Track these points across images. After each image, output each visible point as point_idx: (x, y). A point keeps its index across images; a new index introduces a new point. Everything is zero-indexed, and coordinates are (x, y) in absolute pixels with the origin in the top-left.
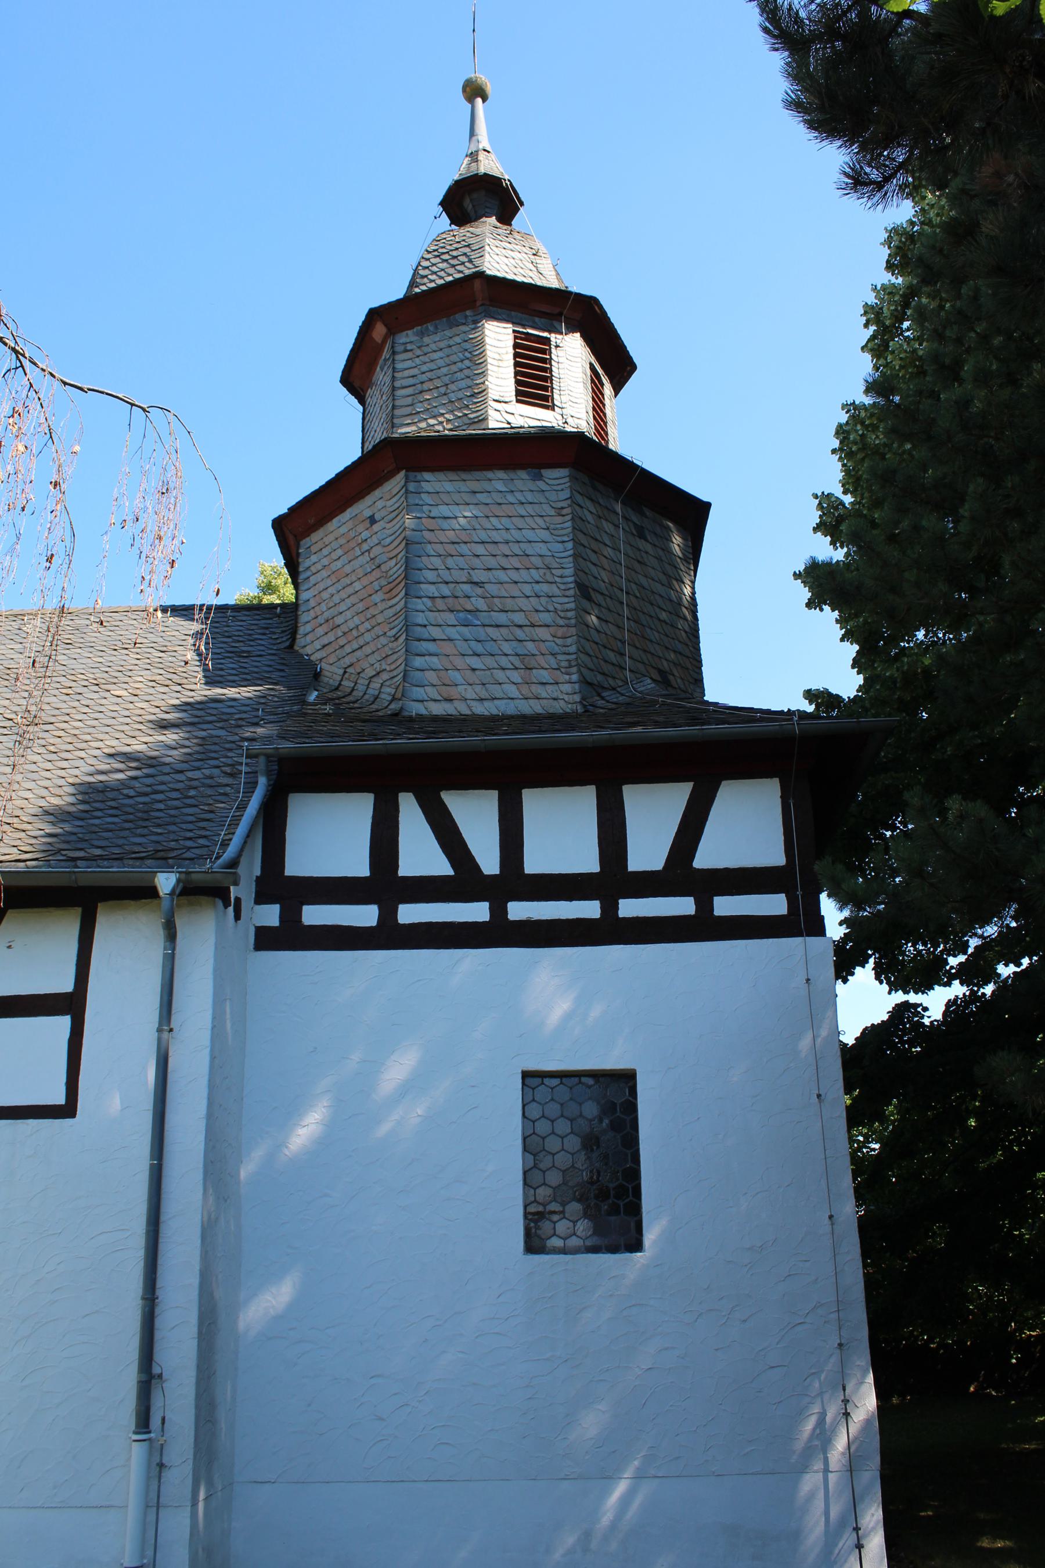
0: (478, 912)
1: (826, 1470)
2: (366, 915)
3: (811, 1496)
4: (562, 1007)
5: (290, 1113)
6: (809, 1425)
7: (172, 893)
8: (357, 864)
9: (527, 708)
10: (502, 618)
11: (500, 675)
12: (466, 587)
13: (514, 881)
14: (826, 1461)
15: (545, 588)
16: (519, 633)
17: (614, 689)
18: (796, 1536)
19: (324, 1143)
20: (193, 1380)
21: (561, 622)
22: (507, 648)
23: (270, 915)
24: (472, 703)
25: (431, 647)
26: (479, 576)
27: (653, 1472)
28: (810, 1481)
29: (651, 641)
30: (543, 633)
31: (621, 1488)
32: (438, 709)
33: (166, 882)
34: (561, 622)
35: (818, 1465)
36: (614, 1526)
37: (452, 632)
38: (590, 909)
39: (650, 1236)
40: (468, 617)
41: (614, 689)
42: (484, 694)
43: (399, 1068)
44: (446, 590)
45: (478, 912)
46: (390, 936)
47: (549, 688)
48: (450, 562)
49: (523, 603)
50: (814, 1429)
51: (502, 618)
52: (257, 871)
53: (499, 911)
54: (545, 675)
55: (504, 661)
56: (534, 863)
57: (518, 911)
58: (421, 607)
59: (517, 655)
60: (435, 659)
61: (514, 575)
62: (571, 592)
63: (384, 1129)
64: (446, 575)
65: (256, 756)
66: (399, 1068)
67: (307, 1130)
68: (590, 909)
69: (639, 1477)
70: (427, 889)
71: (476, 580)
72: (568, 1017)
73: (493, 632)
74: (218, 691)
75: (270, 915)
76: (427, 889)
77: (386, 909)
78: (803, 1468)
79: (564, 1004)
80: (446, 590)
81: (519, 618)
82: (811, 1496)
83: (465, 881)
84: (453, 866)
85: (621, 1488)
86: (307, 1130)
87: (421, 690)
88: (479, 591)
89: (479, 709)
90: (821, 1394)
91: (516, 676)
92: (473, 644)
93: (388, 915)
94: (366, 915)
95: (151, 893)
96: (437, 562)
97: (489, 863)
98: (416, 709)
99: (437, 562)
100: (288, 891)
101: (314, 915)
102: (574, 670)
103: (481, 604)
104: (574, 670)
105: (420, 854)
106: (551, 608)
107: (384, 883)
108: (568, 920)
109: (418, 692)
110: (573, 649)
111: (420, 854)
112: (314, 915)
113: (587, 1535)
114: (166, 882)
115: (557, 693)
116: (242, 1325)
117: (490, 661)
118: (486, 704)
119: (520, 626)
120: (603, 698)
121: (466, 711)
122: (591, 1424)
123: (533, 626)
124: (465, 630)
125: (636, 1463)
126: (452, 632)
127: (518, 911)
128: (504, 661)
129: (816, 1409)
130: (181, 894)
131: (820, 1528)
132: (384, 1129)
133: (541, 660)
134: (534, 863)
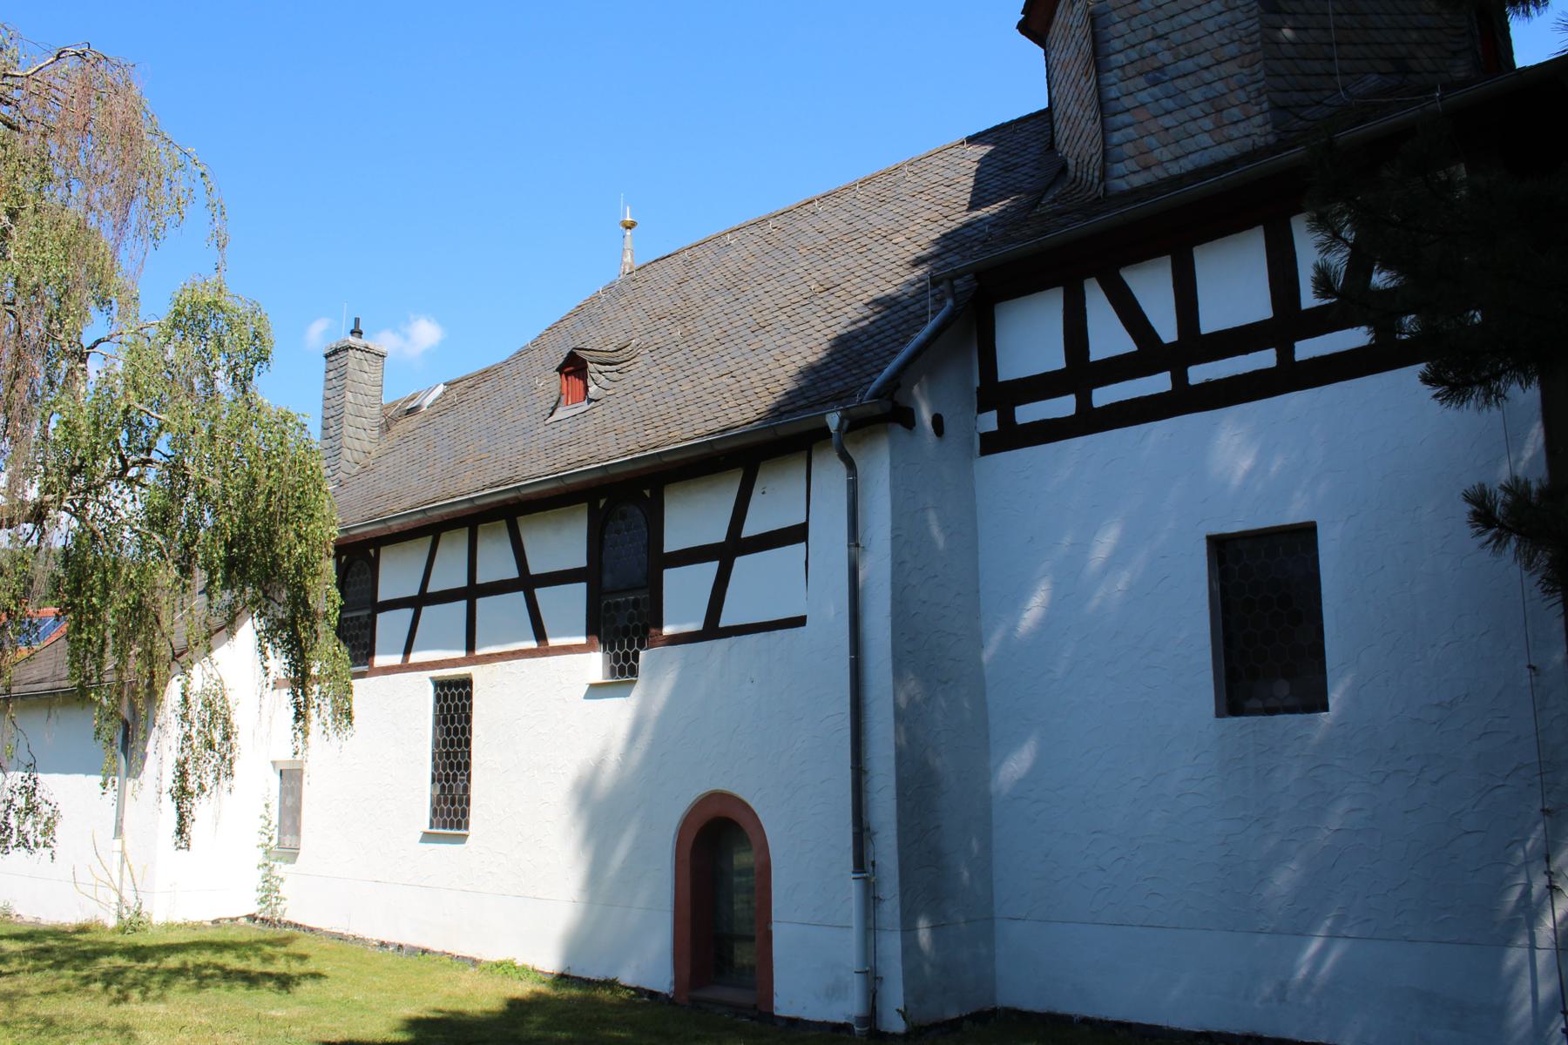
0: (1160, 383)
1: (1533, 947)
2: (1065, 406)
3: (1516, 973)
4: (1245, 463)
5: (1017, 601)
6: (1514, 895)
7: (839, 429)
8: (1052, 358)
9: (1229, 150)
10: (1189, 65)
11: (1192, 127)
12: (1152, 44)
13: (1196, 344)
14: (1532, 937)
15: (1227, 17)
16: (1207, 76)
17: (1318, 103)
18: (1501, 1011)
19: (1046, 623)
20: (895, 848)
21: (1248, 49)
22: (1196, 95)
23: (989, 421)
24: (1168, 165)
25: (1126, 118)
26: (1161, 29)
27: (1344, 932)
28: (1515, 955)
29: (1377, 29)
30: (1231, 68)
31: (1314, 946)
32: (1138, 181)
33: (833, 420)
34: (1248, 49)
35: (1523, 940)
36: (1308, 982)
37: (1143, 96)
38: (1265, 359)
39: (1334, 698)
40: (1156, 77)
41: (1318, 103)
42: (1179, 152)
43: (1105, 543)
44: (1133, 54)
45: (1160, 383)
46: (1089, 421)
47: (1241, 125)
48: (1135, 23)
49: (1207, 42)
50: (1518, 901)
51: (1189, 65)
52: (977, 383)
53: (1180, 378)
54: (1236, 112)
55: (1195, 111)
56: (1211, 321)
57: (1199, 374)
58: (1114, 80)
59: (1207, 100)
60: (1130, 130)
61: (1196, 15)
62: (1255, 12)
63: (1094, 603)
64: (1132, 39)
65: (940, 282)
66: (1105, 543)
67: (1035, 608)
68: (1265, 359)
69: (1332, 936)
70: (1118, 369)
71: (1160, 32)
72: (1250, 474)
73: (1180, 83)
74: (975, 214)
75: (989, 421)
76: (1118, 369)
77: (1085, 398)
78: (1508, 942)
79: (1244, 464)
80: (1133, 54)
81: (1204, 60)
82: (1516, 973)
83: (1148, 354)
84: (1136, 341)
85: (1314, 946)
86: (1035, 608)
87: (1120, 165)
88: (1164, 44)
89: (1175, 169)
90: (1526, 863)
91: (1208, 123)
92: (1164, 102)
93: (1084, 401)
94: (1065, 406)
95: (824, 433)
96: (1122, 27)
97: (1167, 331)
98: (1122, 185)
99: (1122, 27)
100: (1002, 395)
101: (1026, 414)
102: (1264, 97)
103: (1166, 57)
104: (1264, 97)
105: (1108, 337)
106: (1236, 37)
107: (1081, 373)
108: (1245, 375)
109: (1120, 168)
110: (1261, 75)
111: (1108, 337)
112: (1026, 414)
113: (1283, 987)
114: (833, 420)
115: (1249, 129)
116: (993, 788)
117: (1181, 116)
118: (1182, 162)
119: (1207, 68)
120: (1302, 119)
121: (1164, 175)
122: (1284, 879)
123: (1219, 63)
124: (1155, 90)
125: (1328, 923)
126: (1143, 96)
127: (1199, 374)
128: (1195, 111)
129: (1522, 880)
130: (850, 429)
131: (1527, 1007)
132: (1094, 603)
133: (1232, 99)
134: (1211, 321)
